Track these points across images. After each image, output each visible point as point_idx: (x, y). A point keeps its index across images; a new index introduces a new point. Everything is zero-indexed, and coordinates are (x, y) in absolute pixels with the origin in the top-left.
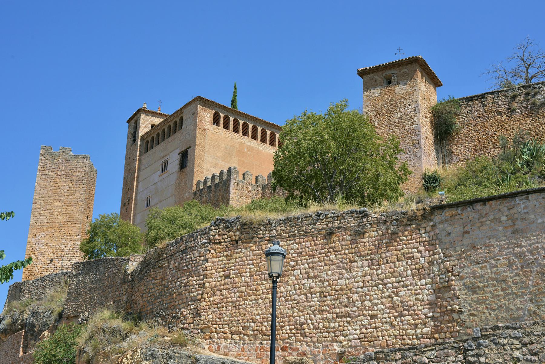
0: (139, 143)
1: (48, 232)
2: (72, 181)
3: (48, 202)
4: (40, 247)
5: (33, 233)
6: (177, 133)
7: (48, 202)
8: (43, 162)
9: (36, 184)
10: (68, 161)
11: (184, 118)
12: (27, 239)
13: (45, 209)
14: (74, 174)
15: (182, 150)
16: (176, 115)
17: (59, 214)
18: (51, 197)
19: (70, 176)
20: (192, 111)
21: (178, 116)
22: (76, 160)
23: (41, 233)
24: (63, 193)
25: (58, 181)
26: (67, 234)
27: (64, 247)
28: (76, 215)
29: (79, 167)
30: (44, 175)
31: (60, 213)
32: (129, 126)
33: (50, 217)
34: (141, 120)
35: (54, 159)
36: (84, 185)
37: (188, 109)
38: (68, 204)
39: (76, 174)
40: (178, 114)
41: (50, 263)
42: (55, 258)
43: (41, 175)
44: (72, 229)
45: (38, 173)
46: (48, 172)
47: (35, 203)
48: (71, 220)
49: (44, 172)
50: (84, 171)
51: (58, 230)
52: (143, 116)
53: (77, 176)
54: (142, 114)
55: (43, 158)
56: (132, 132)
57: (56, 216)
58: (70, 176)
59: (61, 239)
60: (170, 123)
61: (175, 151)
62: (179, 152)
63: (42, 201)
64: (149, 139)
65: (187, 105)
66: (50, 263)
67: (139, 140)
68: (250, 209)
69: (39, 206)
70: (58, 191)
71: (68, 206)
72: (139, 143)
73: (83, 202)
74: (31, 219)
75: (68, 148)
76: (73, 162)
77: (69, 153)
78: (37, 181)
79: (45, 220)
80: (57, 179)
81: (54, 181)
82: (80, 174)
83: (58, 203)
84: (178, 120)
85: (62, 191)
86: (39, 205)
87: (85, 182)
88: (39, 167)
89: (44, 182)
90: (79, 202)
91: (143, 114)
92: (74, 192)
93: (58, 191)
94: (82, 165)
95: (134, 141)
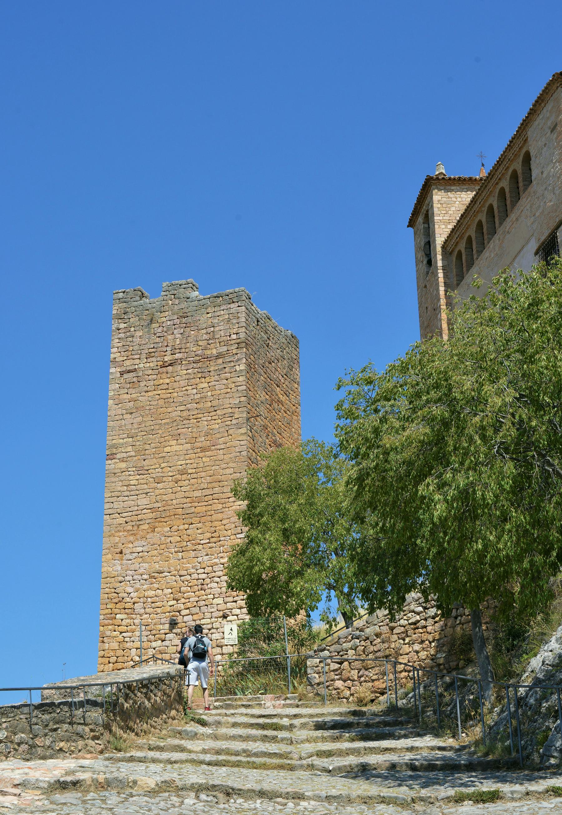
0: (440, 264)
1: (155, 538)
2: (206, 374)
3: (147, 447)
4: (138, 585)
5: (115, 546)
6: (524, 197)
7: (147, 447)
8: (122, 335)
9: (110, 402)
10: (189, 319)
11: (532, 154)
12: (101, 567)
13: (141, 471)
14: (208, 352)
15: (543, 238)
16: (510, 155)
17: (179, 477)
18: (152, 432)
19: (199, 361)
20: (549, 123)
21: (516, 156)
22: (209, 310)
23: (136, 544)
24: (185, 414)
25: (167, 381)
26: (209, 535)
27: (204, 576)
28: (228, 471)
29: (221, 330)
30: (129, 372)
31: (183, 473)
32: (415, 233)
33: (157, 492)
34: (436, 206)
35: (151, 320)
36: (241, 379)
37: (536, 123)
38: (202, 441)
39: (214, 352)
40: (516, 148)
41: (171, 630)
42: (184, 612)
43: (122, 374)
44: (220, 516)
45: (112, 370)
46: (137, 361)
47: (111, 457)
48: (216, 490)
49: (128, 363)
50: (234, 337)
51: (181, 527)
52: (438, 196)
53: (218, 357)
54: (435, 191)
55: (122, 326)
56: (423, 244)
57: (171, 484)
58: (199, 361)
59: (193, 554)
60: (501, 185)
61: (525, 249)
62: (534, 250)
63: (130, 449)
64: (462, 246)
65: (533, 112)
66: (171, 630)
67: (439, 257)
68: (287, 803)
69: (123, 465)
70: (170, 410)
71: (203, 450)
72: (440, 264)
73: (243, 430)
74: (107, 506)
75: (183, 281)
76: (203, 319)
77: (188, 295)
78: (111, 394)
79: (143, 501)
80: (164, 376)
81: (156, 383)
82: (225, 348)
83: (174, 447)
84: (518, 165)
85: (182, 408)
86: (122, 460)
87: (242, 367)
88: (114, 354)
89: (131, 391)
90: (231, 432)
91: (440, 190)
92: (215, 403)
93: (170, 410)
94: (229, 320)
95: (430, 263)
